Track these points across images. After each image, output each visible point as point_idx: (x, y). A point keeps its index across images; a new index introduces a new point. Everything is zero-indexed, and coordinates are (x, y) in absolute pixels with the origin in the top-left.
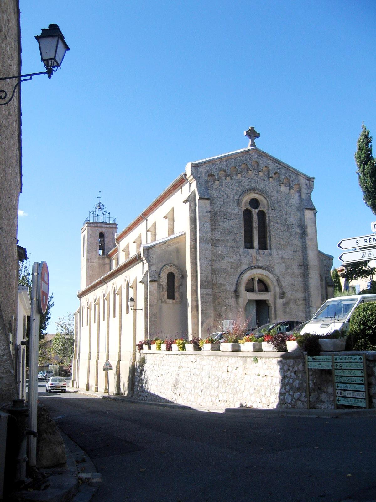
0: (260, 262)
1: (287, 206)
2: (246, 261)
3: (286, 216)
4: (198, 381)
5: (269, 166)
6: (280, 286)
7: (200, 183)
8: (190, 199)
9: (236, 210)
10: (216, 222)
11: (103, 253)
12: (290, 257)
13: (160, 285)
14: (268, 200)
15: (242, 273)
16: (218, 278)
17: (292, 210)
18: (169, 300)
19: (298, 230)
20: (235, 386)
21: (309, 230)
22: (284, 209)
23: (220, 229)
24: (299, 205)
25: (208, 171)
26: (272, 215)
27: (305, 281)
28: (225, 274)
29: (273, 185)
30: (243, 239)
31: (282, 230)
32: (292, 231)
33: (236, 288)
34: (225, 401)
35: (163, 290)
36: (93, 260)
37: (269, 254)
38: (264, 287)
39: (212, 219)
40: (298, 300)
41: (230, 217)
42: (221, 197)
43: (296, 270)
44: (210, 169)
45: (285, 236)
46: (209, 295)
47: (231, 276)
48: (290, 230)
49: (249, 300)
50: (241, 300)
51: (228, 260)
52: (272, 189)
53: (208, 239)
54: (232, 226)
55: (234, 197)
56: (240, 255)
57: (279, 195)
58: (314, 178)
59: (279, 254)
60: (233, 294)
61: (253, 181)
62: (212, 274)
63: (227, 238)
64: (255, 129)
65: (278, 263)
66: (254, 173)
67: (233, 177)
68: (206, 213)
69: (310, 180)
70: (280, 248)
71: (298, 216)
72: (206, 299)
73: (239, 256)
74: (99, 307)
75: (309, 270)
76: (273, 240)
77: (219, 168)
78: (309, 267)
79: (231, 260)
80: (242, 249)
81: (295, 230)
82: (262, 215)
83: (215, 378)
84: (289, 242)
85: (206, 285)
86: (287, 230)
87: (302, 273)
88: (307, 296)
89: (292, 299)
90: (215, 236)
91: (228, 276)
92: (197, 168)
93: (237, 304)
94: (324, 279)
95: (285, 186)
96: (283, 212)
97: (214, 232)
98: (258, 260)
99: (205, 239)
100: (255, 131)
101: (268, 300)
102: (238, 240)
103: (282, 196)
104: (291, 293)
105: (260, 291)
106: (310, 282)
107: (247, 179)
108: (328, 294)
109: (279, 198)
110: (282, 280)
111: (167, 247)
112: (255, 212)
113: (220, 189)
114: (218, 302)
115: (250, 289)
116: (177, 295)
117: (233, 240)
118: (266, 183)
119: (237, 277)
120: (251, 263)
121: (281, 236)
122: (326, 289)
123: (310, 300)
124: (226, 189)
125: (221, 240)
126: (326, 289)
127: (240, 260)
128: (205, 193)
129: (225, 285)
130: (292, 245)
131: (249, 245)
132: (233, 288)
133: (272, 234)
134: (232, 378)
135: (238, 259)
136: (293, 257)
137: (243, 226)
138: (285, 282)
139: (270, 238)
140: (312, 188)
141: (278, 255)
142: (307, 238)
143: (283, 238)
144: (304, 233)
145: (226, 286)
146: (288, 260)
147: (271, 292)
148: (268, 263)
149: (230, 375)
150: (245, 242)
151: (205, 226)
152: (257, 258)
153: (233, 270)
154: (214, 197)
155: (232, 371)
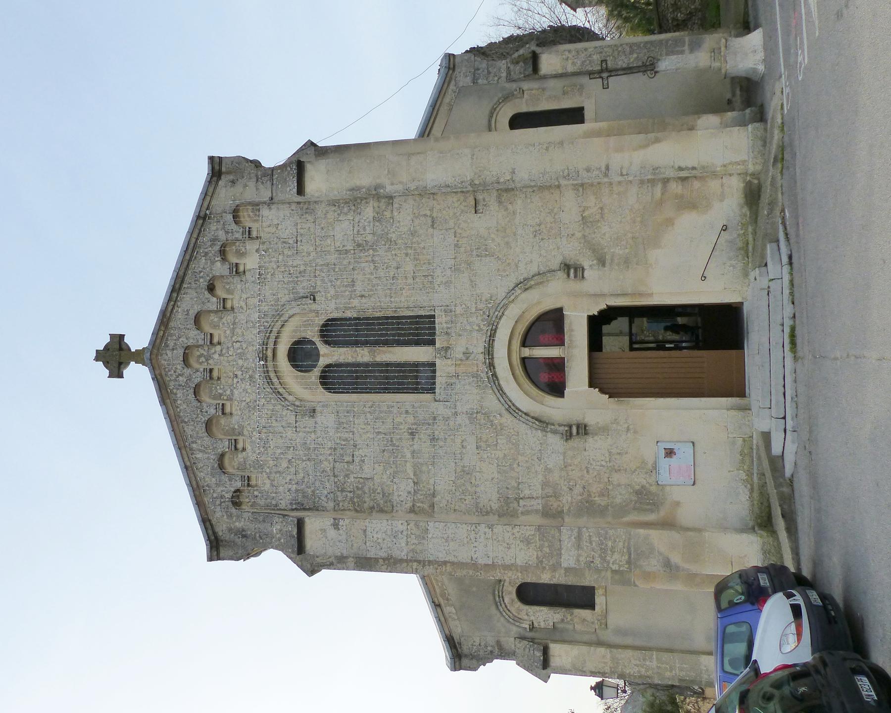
5: (192, 313)
6: (541, 276)
8: (309, 566)
9: (325, 419)
12: (451, 239)
13: (557, 634)
15: (512, 409)
16: (527, 492)
19: (369, 211)
22: (311, 258)
23: (385, 477)
28: (513, 469)
29: (244, 296)
35: (568, 623)
38: (550, 325)
39: (358, 509)
40: (586, 214)
41: (346, 440)
42: (292, 470)
44: (218, 502)
48: (369, 238)
49: (592, 384)
50: (591, 419)
53: (415, 531)
56: (456, 414)
58: (211, 159)
61: (240, 362)
63: (409, 455)
65: (473, 285)
67: (236, 427)
68: (341, 532)
73: (459, 418)
81: (369, 222)
82: (331, 331)
87: (499, 197)
89: (584, 236)
90: (404, 495)
93: (604, 430)
94: (514, 86)
100: (107, 348)
102: (410, 419)
104: (564, 239)
105: (559, 339)
106: (526, 177)
107: (235, 380)
108: (560, 72)
110: (524, 271)
112: (328, 355)
115: (552, 379)
118: (242, 317)
124: (270, 451)
126: (545, 77)
129: (548, 470)
130: (413, 234)
132: (555, 441)
135: (467, 422)
138: (531, 262)
143: (395, 265)
146: (462, 250)
152: (461, 356)
154: (297, 491)
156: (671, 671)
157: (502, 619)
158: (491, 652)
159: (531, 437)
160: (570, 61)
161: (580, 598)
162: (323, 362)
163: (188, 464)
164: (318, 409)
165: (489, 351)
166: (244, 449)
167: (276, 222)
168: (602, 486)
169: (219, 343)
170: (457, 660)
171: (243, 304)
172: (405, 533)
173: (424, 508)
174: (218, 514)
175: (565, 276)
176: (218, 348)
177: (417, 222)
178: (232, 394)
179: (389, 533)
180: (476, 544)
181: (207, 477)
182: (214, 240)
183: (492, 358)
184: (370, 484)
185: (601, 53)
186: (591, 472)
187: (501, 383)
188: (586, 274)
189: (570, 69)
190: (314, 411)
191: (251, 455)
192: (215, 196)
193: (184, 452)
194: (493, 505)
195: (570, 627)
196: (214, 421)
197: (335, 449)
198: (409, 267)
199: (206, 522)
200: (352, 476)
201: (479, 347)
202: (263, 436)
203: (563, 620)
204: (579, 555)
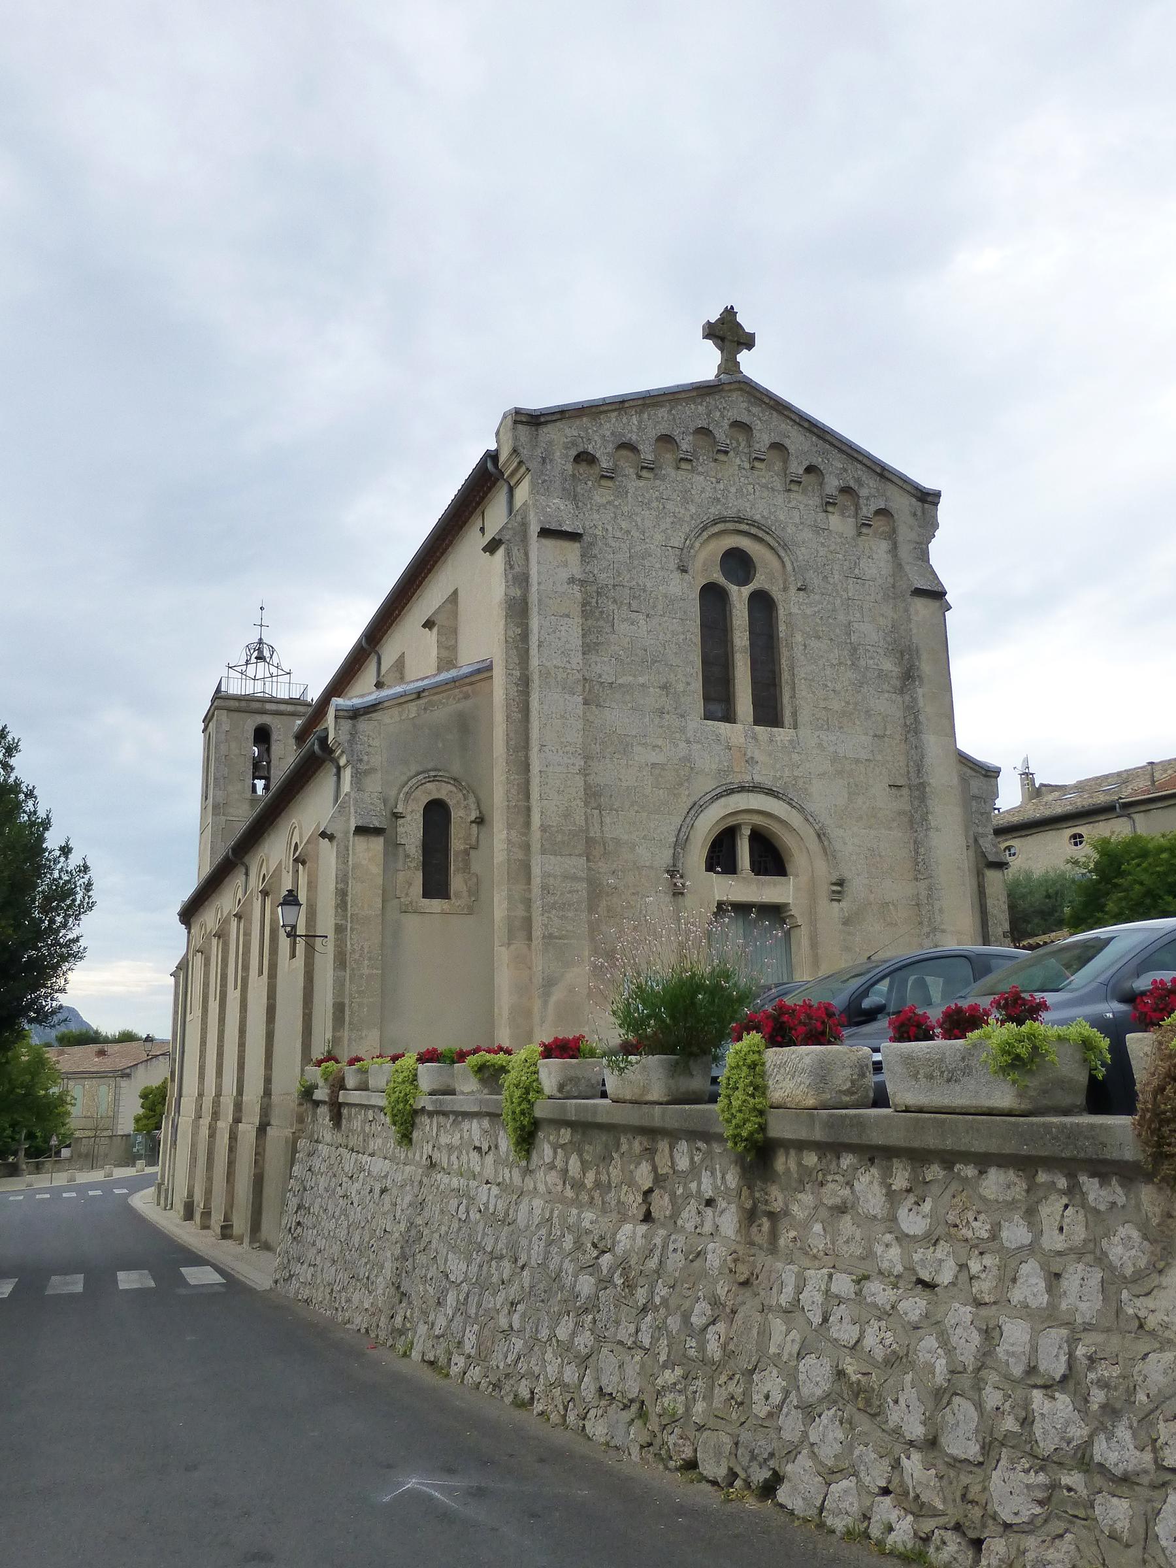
2: (708, 762)
4: (497, 1253)
5: (787, 442)
6: (828, 853)
8: (507, 537)
10: (601, 623)
11: (266, 788)
12: (864, 755)
13: (393, 847)
14: (786, 559)
15: (696, 808)
16: (608, 820)
18: (427, 901)
19: (888, 665)
20: (697, 1320)
21: (926, 667)
24: (891, 580)
25: (574, 444)
27: (915, 842)
28: (632, 805)
29: (802, 507)
30: (697, 685)
32: (867, 668)
33: (675, 857)
34: (632, 1401)
36: (231, 810)
37: (791, 741)
38: (770, 858)
39: (588, 610)
41: (654, 607)
43: (886, 802)
44: (582, 434)
46: (575, 878)
48: (862, 663)
50: (689, 900)
52: (797, 520)
55: (668, 538)
56: (688, 742)
59: (825, 744)
61: (733, 490)
62: (586, 804)
63: (641, 680)
64: (740, 319)
66: (738, 461)
68: (566, 586)
69: (928, 499)
73: (683, 745)
74: (226, 946)
75: (929, 802)
76: (804, 693)
77: (612, 434)
78: (927, 789)
79: (654, 757)
80: (695, 721)
82: (762, 603)
83: (578, 1246)
84: (856, 704)
86: (849, 663)
87: (904, 813)
88: (924, 893)
90: (598, 669)
95: (842, 514)
97: (593, 658)
98: (751, 761)
99: (561, 675)
101: (787, 904)
107: (714, 480)
109: (821, 554)
110: (835, 833)
111: (425, 709)
112: (739, 596)
115: (721, 855)
116: (457, 882)
117: (665, 687)
119: (678, 820)
122: (980, 875)
123: (937, 907)
125: (621, 685)
127: (687, 759)
129: (633, 847)
131: (717, 708)
132: (665, 857)
133: (801, 673)
134: (676, 1261)
135: (681, 755)
137: (698, 640)
139: (793, 689)
140: (935, 526)
142: (920, 691)
144: (909, 676)
146: (853, 766)
147: (797, 876)
148: (787, 773)
149: (665, 1246)
150: (707, 698)
152: (749, 754)
154: (596, 536)
155: (675, 1216)
156: (359, 992)
157: (404, 778)
158: (361, 760)
159: (667, 829)
161: (436, 884)
162: (733, 589)
163: (627, 405)
164: (686, 576)
165: (756, 788)
166: (639, 477)
167: (875, 556)
168: (619, 910)
169: (752, 468)
170: (351, 714)
171: (793, 504)
172: (568, 666)
173: (593, 694)
174: (567, 431)
175: (834, 881)
176: (747, 466)
177: (879, 718)
178: (698, 474)
179: (567, 646)
180: (560, 752)
181: (610, 425)
182: (858, 481)
183: (749, 791)
184: (608, 629)
186: (634, 898)
187: (723, 799)
188: (835, 904)
190: (686, 571)
191: (633, 484)
192: (901, 492)
193: (640, 402)
194: (592, 777)
195: (400, 866)
196: (669, 446)
197: (645, 591)
198: (836, 705)
199: (562, 414)
200: (615, 607)
201: (762, 776)
202: (655, 504)
203: (407, 856)
204: (555, 877)
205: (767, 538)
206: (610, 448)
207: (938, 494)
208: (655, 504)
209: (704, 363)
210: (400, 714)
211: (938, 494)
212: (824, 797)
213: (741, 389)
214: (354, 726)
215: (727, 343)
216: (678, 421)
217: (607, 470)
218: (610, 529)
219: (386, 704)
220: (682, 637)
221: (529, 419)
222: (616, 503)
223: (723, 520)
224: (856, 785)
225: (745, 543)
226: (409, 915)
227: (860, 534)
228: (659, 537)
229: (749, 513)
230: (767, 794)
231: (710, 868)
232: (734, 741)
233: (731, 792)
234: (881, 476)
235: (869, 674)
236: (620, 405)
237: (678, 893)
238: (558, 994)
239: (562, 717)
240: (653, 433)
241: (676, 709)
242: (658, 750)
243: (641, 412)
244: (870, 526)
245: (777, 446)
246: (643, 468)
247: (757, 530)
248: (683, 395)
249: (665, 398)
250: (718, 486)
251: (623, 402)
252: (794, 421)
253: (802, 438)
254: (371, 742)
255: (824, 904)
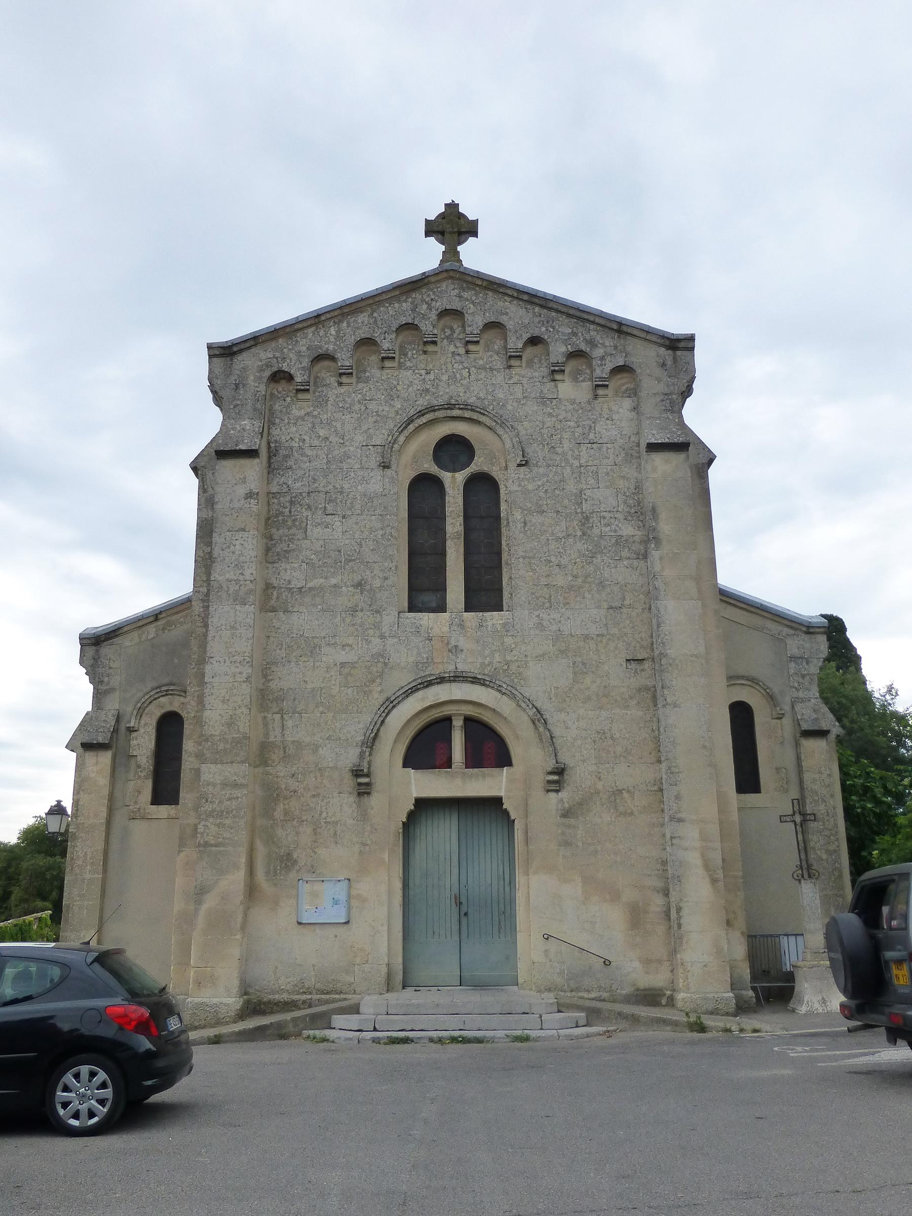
0: (462, 656)
1: (583, 447)
3: (580, 482)
5: (503, 319)
7: (235, 406)
8: (203, 464)
9: (376, 482)
10: (293, 531)
12: (594, 630)
15: (390, 705)
16: (290, 723)
17: (605, 461)
25: (269, 365)
26: (520, 485)
28: (317, 707)
29: (525, 381)
31: (560, 535)
32: (601, 537)
35: (136, 773)
37: (504, 625)
44: (277, 354)
45: (573, 557)
46: (236, 785)
47: (344, 716)
48: (596, 531)
50: (376, 801)
51: (332, 656)
52: (520, 395)
54: (357, 536)
55: (370, 437)
56: (382, 637)
57: (550, 415)
60: (349, 782)
63: (333, 581)
65: (540, 657)
67: (367, 374)
68: (243, 501)
69: (680, 346)
70: (550, 602)
71: (628, 479)
72: (221, 802)
73: (376, 641)
76: (521, 572)
80: (389, 618)
82: (483, 487)
85: (225, 750)
86: (579, 533)
91: (330, 715)
92: (232, 360)
93: (364, 816)
95: (575, 379)
96: (568, 471)
99: (233, 588)
100: (462, 216)
103: (563, 415)
107: (423, 372)
109: (548, 424)
110: (555, 719)
112: (454, 483)
113: (316, 417)
114: (286, 813)
115: (426, 746)
117: (359, 585)
120: (430, 661)
121: (553, 559)
122: (797, 745)
128: (245, 434)
129: (316, 748)
130: (601, 585)
132: (350, 757)
135: (375, 651)
136: (605, 632)
141: (540, 626)
145: (321, 751)
146: (581, 644)
151: (235, 545)
152: (453, 643)
153: (350, 691)
154: (291, 448)
159: (355, 728)
160: (817, 776)
161: (165, 789)
162: (446, 477)
163: (323, 318)
164: (388, 472)
165: (457, 678)
166: (340, 384)
167: (615, 417)
169: (467, 352)
171: (514, 380)
172: (241, 578)
174: (263, 355)
175: (549, 769)
176: (462, 351)
179: (242, 559)
182: (592, 343)
183: (450, 681)
185: (828, 815)
186: (314, 800)
188: (553, 795)
189: (807, 776)
190: (388, 467)
191: (333, 393)
192: (646, 344)
195: (131, 775)
197: (342, 493)
198: (560, 580)
199: (255, 340)
200: (309, 513)
201: (464, 665)
202: (357, 407)
203: (139, 766)
204: (214, 785)
205: (482, 419)
206: (306, 362)
207: (691, 338)
208: (357, 407)
209: (429, 255)
210: (140, 636)
211: (691, 338)
212: (542, 681)
213: (452, 278)
214: (97, 651)
215: (447, 236)
216: (379, 323)
217: (302, 383)
218: (307, 438)
219: (125, 629)
220: (381, 532)
221: (222, 351)
222: (315, 413)
223: (432, 409)
224: (584, 664)
225: (461, 428)
226: (137, 822)
227: (596, 397)
228: (360, 438)
229: (463, 398)
230: (472, 682)
231: (405, 765)
232: (436, 631)
233: (429, 684)
234: (619, 331)
235: (603, 543)
236: (317, 320)
237: (364, 790)
238: (210, 902)
239: (232, 627)
240: (351, 340)
241: (370, 605)
242: (347, 648)
243: (341, 321)
244: (607, 386)
245: (493, 326)
246: (341, 375)
247: (470, 412)
248: (384, 297)
249: (364, 303)
250: (428, 377)
251: (318, 316)
252: (512, 296)
253: (522, 312)
254: (112, 664)
255: (538, 794)
